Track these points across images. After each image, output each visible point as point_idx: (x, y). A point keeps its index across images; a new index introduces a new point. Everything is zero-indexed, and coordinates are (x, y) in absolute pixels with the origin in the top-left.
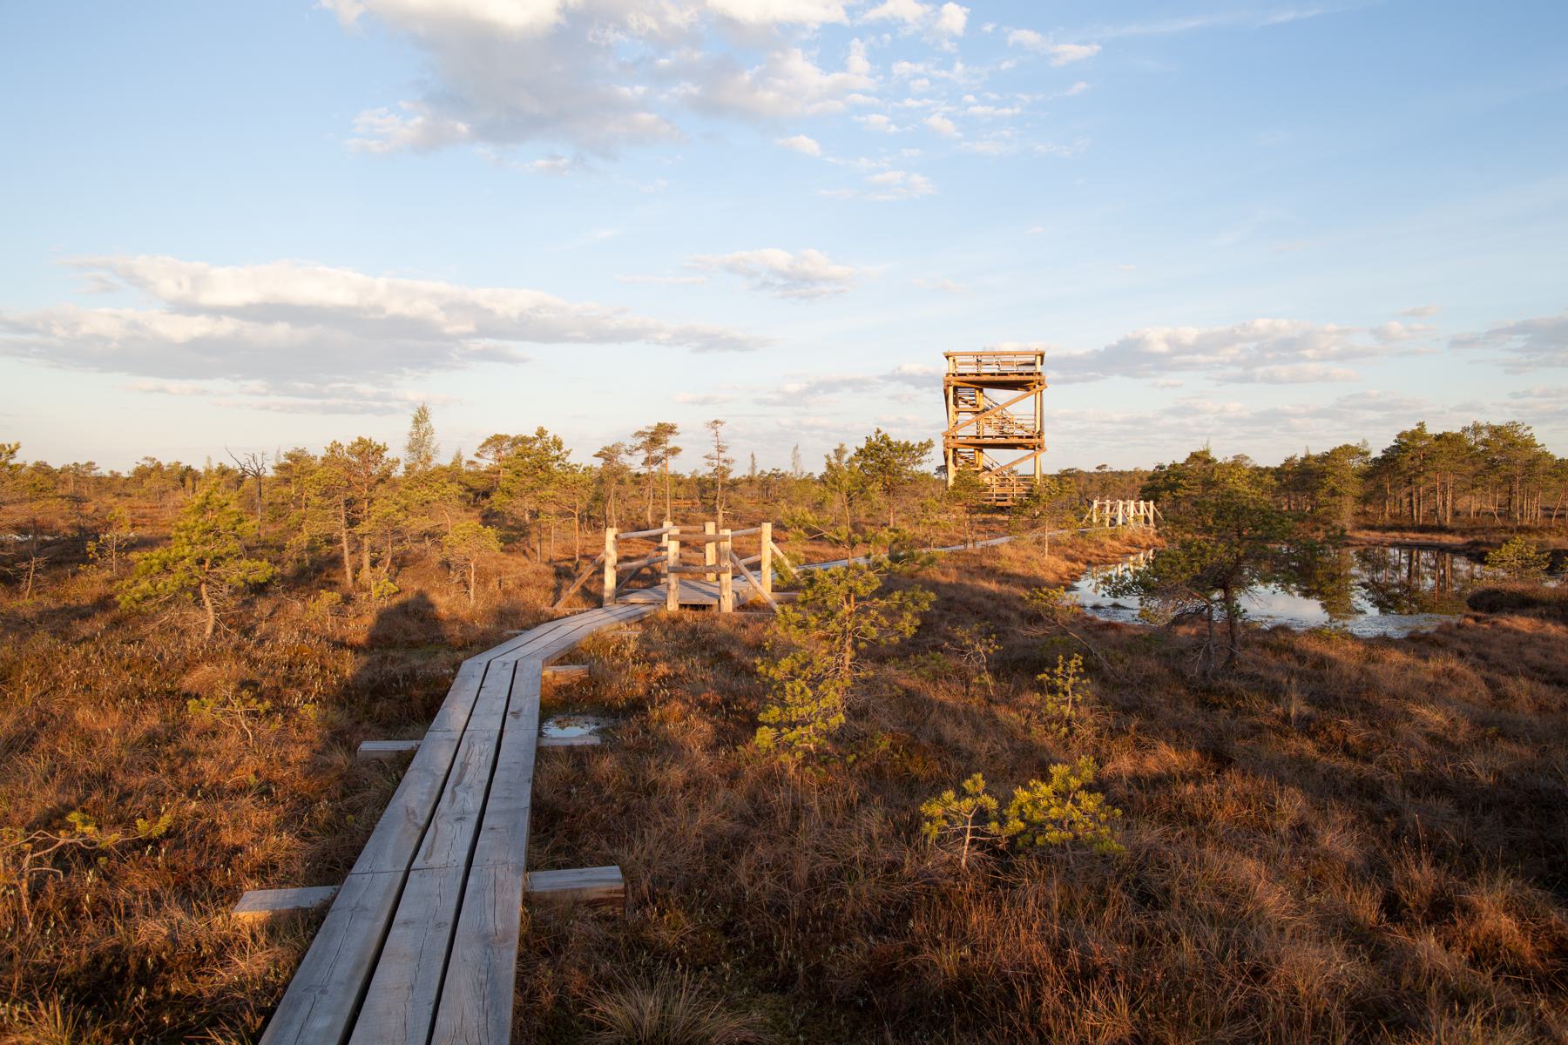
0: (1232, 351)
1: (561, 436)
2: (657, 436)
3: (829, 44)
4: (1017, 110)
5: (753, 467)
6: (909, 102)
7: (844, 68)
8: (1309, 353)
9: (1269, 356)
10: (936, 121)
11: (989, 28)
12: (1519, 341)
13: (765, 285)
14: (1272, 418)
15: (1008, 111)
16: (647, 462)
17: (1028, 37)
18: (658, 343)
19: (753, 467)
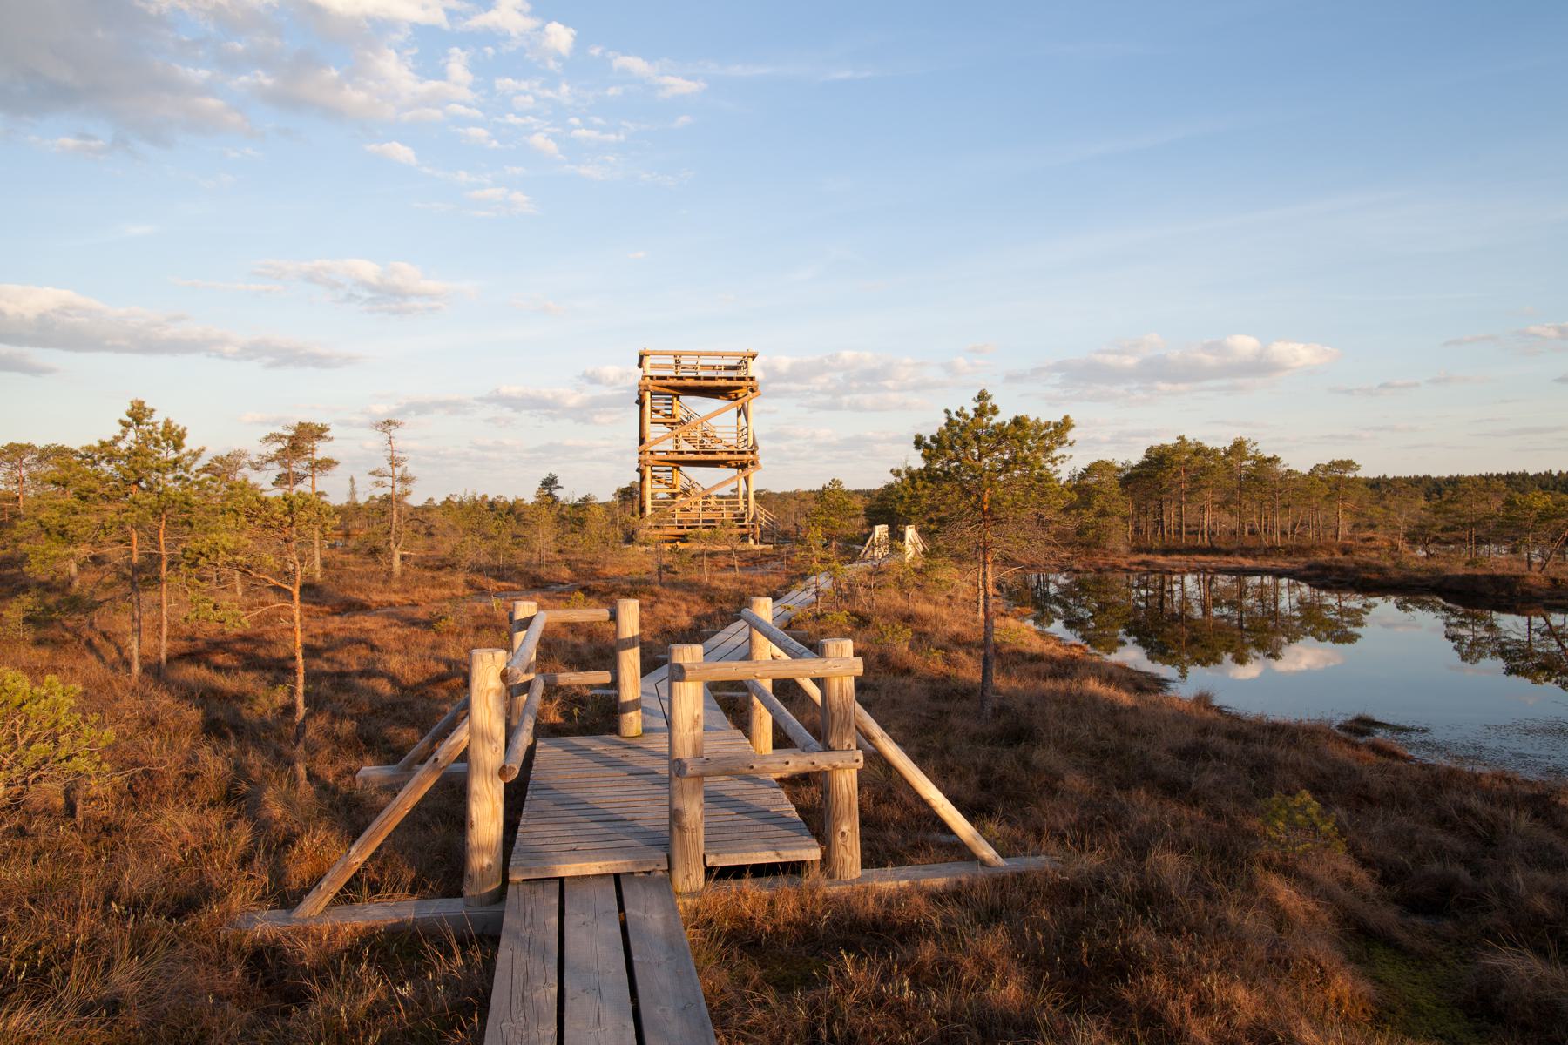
0: (822, 380)
1: (179, 422)
2: (301, 439)
3: (429, 46)
4: (622, 137)
5: (353, 493)
6: (512, 119)
7: (442, 75)
8: (890, 383)
9: (855, 385)
10: (539, 140)
11: (596, 51)
12: (1057, 378)
13: (350, 297)
14: (857, 443)
15: (612, 137)
16: (282, 480)
17: (637, 64)
18: (222, 356)
19: (353, 493)
